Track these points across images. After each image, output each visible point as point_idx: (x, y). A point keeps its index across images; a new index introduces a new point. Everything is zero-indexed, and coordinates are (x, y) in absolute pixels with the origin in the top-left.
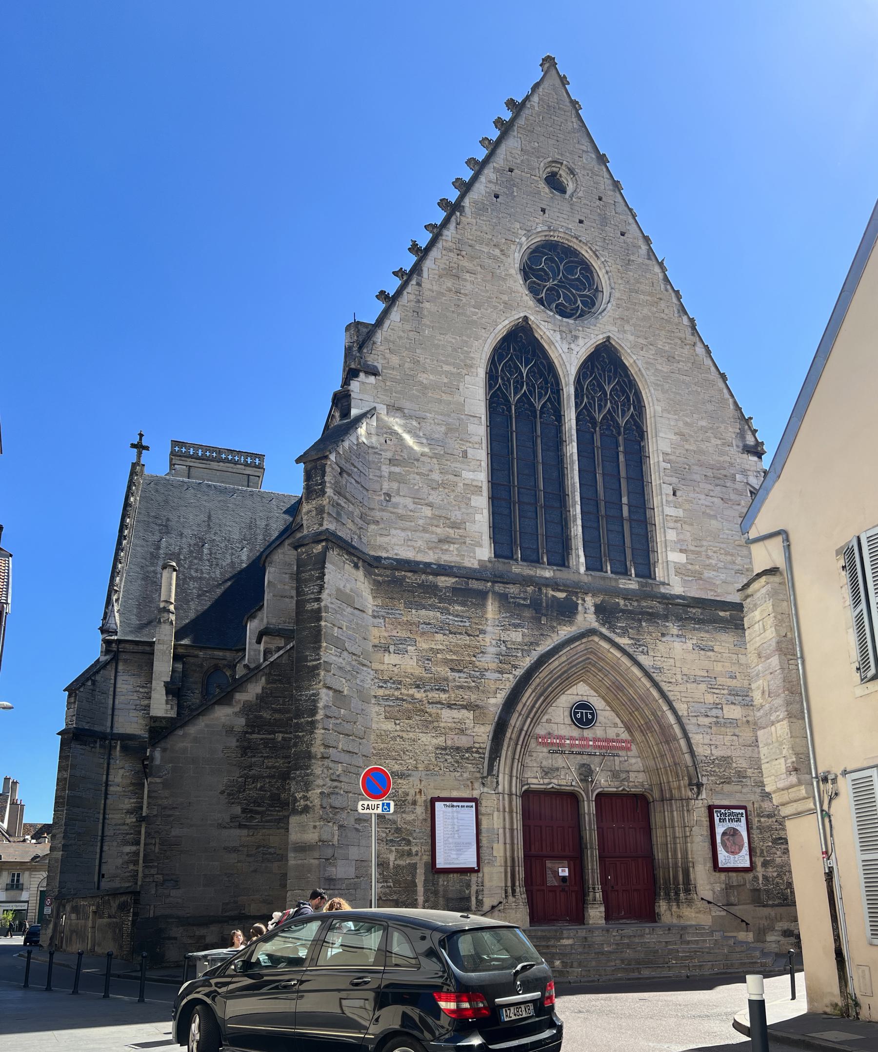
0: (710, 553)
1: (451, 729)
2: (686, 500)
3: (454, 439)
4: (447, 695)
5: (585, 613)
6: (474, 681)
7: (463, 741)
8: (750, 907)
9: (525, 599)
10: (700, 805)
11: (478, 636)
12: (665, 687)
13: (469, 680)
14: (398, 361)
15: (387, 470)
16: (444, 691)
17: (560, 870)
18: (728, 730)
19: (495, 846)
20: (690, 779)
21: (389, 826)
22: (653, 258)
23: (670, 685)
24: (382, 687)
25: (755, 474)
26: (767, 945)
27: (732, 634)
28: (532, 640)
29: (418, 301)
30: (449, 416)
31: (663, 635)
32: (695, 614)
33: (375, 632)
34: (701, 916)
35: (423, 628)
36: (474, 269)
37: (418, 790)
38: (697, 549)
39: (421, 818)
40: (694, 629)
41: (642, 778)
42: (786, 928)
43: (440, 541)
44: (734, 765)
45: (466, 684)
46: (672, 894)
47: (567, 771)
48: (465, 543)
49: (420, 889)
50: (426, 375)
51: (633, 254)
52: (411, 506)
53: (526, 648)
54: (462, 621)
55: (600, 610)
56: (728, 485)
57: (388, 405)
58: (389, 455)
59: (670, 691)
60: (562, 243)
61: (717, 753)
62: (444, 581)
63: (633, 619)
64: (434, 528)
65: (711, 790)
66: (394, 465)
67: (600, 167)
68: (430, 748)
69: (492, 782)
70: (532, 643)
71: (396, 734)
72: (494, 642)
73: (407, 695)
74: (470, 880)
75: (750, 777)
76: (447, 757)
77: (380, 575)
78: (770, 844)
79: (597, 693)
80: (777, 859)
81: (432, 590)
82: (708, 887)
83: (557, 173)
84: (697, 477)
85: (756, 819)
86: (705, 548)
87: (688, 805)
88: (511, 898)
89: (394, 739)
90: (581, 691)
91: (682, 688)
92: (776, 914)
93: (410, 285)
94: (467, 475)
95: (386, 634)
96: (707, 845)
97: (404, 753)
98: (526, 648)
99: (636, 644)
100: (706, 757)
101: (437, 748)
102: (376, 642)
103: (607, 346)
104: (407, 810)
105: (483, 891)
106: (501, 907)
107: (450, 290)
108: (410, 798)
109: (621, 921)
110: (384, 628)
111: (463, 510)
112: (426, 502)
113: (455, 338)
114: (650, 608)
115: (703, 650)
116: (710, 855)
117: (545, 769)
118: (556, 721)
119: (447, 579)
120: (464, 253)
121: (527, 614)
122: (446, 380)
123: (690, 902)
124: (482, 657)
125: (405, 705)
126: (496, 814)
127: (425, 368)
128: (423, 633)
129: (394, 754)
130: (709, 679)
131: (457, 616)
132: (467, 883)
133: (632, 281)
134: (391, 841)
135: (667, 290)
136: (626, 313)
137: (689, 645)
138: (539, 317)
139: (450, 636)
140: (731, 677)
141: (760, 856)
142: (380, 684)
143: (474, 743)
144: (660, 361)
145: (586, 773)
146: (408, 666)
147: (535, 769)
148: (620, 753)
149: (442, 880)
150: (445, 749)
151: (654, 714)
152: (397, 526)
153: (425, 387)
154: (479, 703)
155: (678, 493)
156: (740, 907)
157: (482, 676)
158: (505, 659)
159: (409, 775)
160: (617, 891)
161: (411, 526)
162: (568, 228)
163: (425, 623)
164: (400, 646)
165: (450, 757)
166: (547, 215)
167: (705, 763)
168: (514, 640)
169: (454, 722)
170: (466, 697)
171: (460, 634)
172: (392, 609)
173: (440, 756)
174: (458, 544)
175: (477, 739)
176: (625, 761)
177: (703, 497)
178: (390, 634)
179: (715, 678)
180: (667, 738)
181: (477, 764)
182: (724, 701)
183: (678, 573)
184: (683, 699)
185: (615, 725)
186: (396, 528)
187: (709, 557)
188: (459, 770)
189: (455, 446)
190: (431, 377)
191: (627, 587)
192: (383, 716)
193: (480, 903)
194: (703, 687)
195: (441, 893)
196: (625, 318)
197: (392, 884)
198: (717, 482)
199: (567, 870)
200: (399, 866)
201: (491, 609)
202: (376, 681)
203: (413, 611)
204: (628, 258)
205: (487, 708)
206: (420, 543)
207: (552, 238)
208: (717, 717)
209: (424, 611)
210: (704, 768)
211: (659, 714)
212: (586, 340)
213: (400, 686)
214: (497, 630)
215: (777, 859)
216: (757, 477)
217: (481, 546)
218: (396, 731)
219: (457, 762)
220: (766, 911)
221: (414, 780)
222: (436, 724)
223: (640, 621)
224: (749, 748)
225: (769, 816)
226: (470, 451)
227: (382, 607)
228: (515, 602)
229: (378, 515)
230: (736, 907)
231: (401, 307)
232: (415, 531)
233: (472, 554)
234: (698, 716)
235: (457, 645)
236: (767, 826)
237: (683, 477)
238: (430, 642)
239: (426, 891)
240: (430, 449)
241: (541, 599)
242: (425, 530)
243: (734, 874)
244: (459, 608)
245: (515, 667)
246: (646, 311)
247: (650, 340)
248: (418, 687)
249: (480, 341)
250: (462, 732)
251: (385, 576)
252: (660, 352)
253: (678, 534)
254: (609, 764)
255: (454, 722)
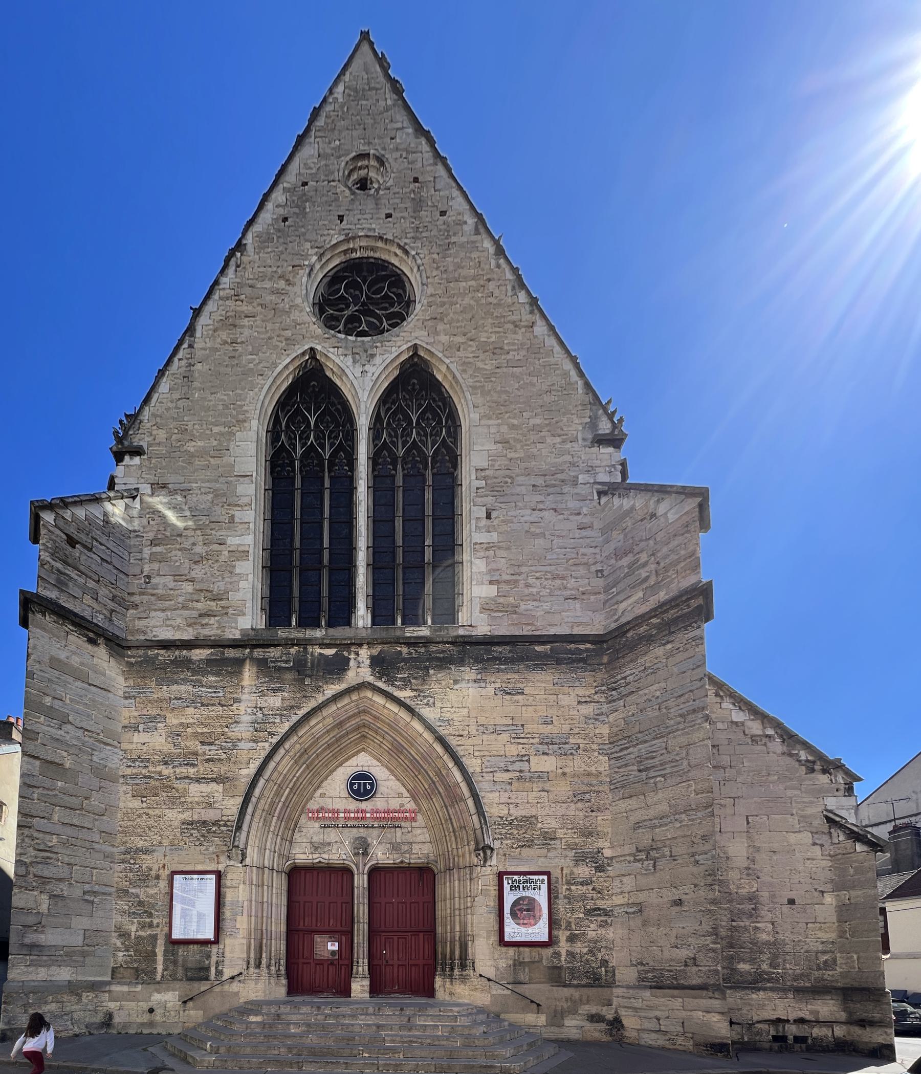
0: (531, 581)
1: (198, 803)
2: (503, 521)
3: (221, 505)
4: (196, 769)
5: (358, 667)
6: (225, 753)
7: (211, 815)
8: (545, 987)
9: (286, 662)
10: (488, 872)
11: (231, 705)
12: (453, 742)
13: (220, 752)
14: (165, 436)
15: (149, 552)
16: (194, 765)
17: (329, 944)
18: (535, 785)
19: (239, 918)
20: (477, 843)
21: (132, 899)
22: (482, 230)
23: (460, 738)
24: (130, 766)
25: (607, 469)
26: (565, 1030)
27: (552, 671)
28: (293, 703)
29: (190, 365)
30: (217, 481)
31: (456, 682)
32: (501, 653)
33: (125, 713)
34: (477, 994)
35: (174, 704)
36: (255, 311)
37: (161, 865)
38: (514, 577)
39: (163, 891)
40: (499, 671)
41: (427, 849)
42: (594, 1012)
43: (200, 615)
44: (539, 825)
45: (216, 757)
46: (447, 970)
47: (340, 845)
48: (227, 614)
49: (160, 958)
50: (194, 443)
51: (455, 234)
52: (172, 585)
53: (285, 712)
54: (215, 692)
55: (375, 662)
56: (565, 491)
57: (152, 484)
58: (151, 536)
59: (460, 745)
60: (368, 258)
61: (516, 813)
62: (199, 654)
63: (418, 668)
64: (195, 604)
65: (505, 855)
66: (156, 545)
67: (418, 140)
68: (176, 824)
69: (237, 855)
70: (292, 707)
71: (142, 811)
72: (249, 710)
73: (155, 772)
74: (210, 952)
75: (561, 839)
76: (193, 831)
77: (133, 657)
78: (582, 915)
79: (380, 762)
80: (590, 933)
81: (186, 663)
82: (489, 963)
83: (366, 179)
84: (523, 490)
85: (564, 887)
86: (525, 574)
87: (471, 874)
88: (252, 970)
89: (140, 816)
90: (363, 762)
91: (477, 741)
92: (581, 996)
93: (182, 350)
94: (233, 541)
95: (136, 714)
96: (493, 918)
97: (149, 829)
98: (285, 712)
99: (419, 695)
100: (502, 818)
101: (183, 824)
102: (126, 722)
103: (416, 364)
104: (150, 884)
105: (223, 961)
106: (242, 978)
107: (225, 343)
108: (153, 873)
109: (393, 996)
110: (134, 708)
111: (227, 579)
112: (188, 577)
113: (228, 395)
114: (440, 653)
115: (509, 694)
116: (496, 928)
117: (315, 844)
118: (331, 795)
119: (201, 651)
120: (243, 297)
121: (289, 676)
122: (215, 443)
123: (464, 979)
124: (235, 727)
125: (153, 782)
126: (242, 886)
127: (193, 435)
128: (173, 709)
129: (139, 830)
130: (514, 728)
131: (210, 687)
132: (207, 954)
133: (451, 268)
134: (134, 913)
135: (498, 266)
136: (441, 310)
137: (490, 689)
138: (326, 345)
139: (202, 708)
140: (545, 723)
141: (566, 929)
142: (129, 764)
143: (222, 816)
144: (482, 356)
145: (362, 848)
146: (157, 744)
147: (304, 845)
148: (403, 824)
149: (181, 951)
150: (192, 823)
151: (439, 773)
152: (156, 607)
153: (192, 456)
154: (229, 775)
155: (494, 514)
156: (532, 986)
157: (235, 746)
158: (260, 727)
159: (154, 851)
160: (392, 965)
161: (170, 605)
162: (370, 230)
163: (176, 698)
164: (149, 724)
165: (196, 831)
166: (345, 222)
167: (499, 825)
168: (272, 705)
169: (203, 797)
170: (216, 769)
171: (213, 705)
172: (143, 688)
173: (186, 831)
174: (219, 616)
175: (225, 812)
176: (409, 832)
177: (529, 512)
178: (141, 713)
179: (523, 725)
180: (454, 798)
181: (225, 837)
182: (532, 751)
183: (483, 609)
184: (477, 754)
185: (400, 795)
186: (155, 610)
187: (528, 586)
188: (204, 843)
189: (220, 513)
190: (199, 443)
191: (415, 634)
192: (130, 795)
193: (219, 973)
194: (505, 737)
195: (181, 962)
196: (439, 317)
197: (133, 953)
198: (551, 490)
199: (337, 944)
200: (140, 936)
201: (248, 674)
202: (125, 760)
203: (165, 687)
204: (447, 241)
205: (238, 779)
206: (179, 621)
207: (354, 255)
208: (521, 771)
209: (175, 686)
210: (498, 831)
211: (444, 772)
212: (385, 357)
213: (147, 764)
214: (254, 697)
215: (590, 933)
216: (610, 472)
217: (244, 614)
218: (142, 808)
219: (203, 836)
220: (566, 992)
221: (158, 855)
222: (183, 799)
223: (427, 668)
224: (563, 805)
225: (583, 884)
226: (237, 514)
227: (133, 687)
228: (275, 667)
229: (136, 599)
230: (526, 986)
231: (170, 376)
232: (175, 609)
233: (233, 625)
234: (496, 771)
235: (209, 717)
236: (579, 895)
237: (502, 493)
238: (180, 717)
239: (165, 961)
240: (195, 521)
241: (306, 660)
242: (185, 607)
243: (527, 950)
244: (213, 679)
245: (272, 734)
246: (467, 301)
247: (469, 335)
248: (166, 763)
249: (256, 390)
250: (209, 805)
251: (138, 657)
252: (484, 348)
253: (487, 564)
254: (389, 836)
255: (203, 797)
